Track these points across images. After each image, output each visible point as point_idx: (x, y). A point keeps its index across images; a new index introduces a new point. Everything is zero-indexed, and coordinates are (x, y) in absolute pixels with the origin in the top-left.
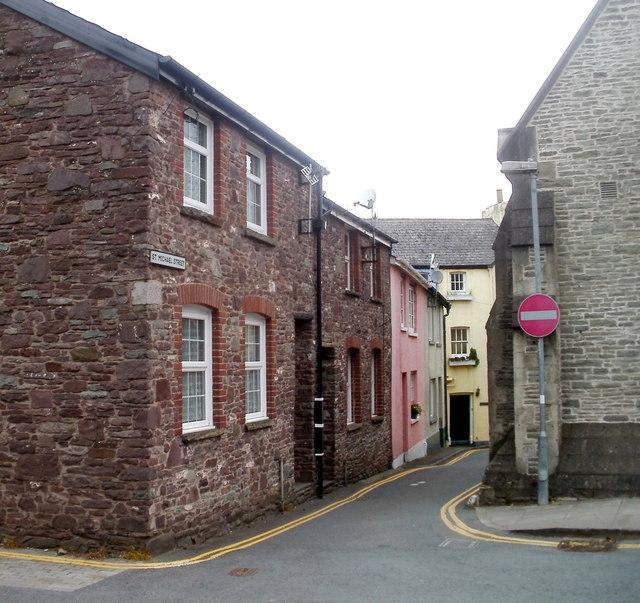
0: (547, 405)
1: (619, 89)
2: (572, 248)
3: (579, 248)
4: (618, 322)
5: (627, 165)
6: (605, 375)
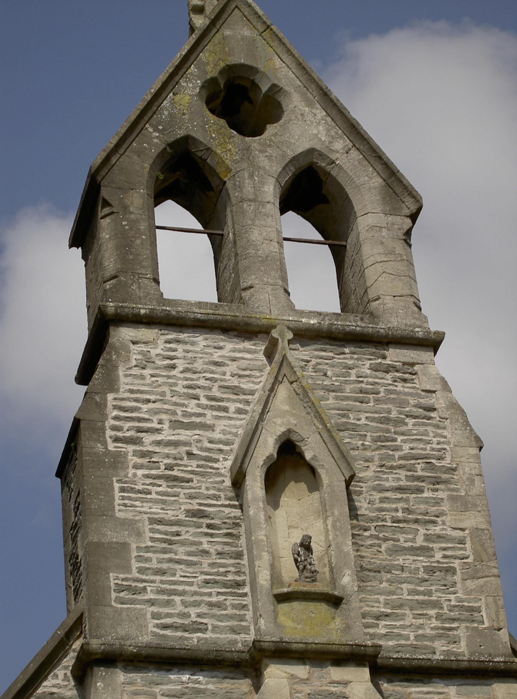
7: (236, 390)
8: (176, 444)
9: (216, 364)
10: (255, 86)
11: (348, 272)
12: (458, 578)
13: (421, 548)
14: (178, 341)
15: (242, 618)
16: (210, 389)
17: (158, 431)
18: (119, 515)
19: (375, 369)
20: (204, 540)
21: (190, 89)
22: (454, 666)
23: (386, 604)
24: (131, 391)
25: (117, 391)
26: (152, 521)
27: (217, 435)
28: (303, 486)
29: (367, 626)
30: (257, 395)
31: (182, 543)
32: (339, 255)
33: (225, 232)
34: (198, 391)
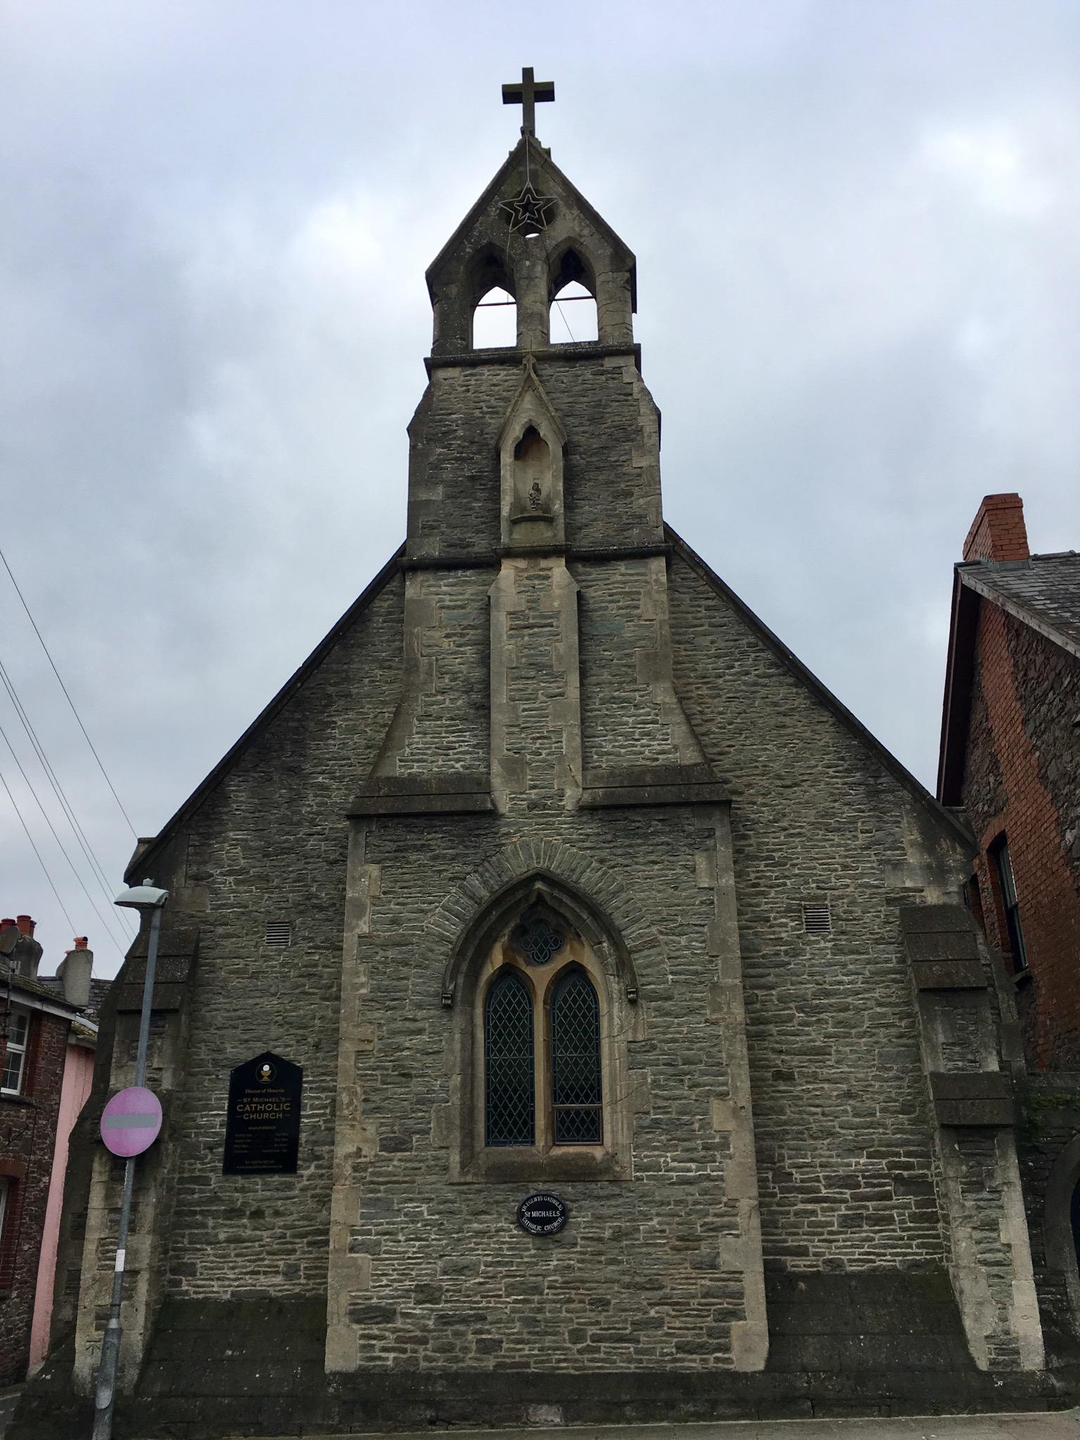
0: (131, 1273)
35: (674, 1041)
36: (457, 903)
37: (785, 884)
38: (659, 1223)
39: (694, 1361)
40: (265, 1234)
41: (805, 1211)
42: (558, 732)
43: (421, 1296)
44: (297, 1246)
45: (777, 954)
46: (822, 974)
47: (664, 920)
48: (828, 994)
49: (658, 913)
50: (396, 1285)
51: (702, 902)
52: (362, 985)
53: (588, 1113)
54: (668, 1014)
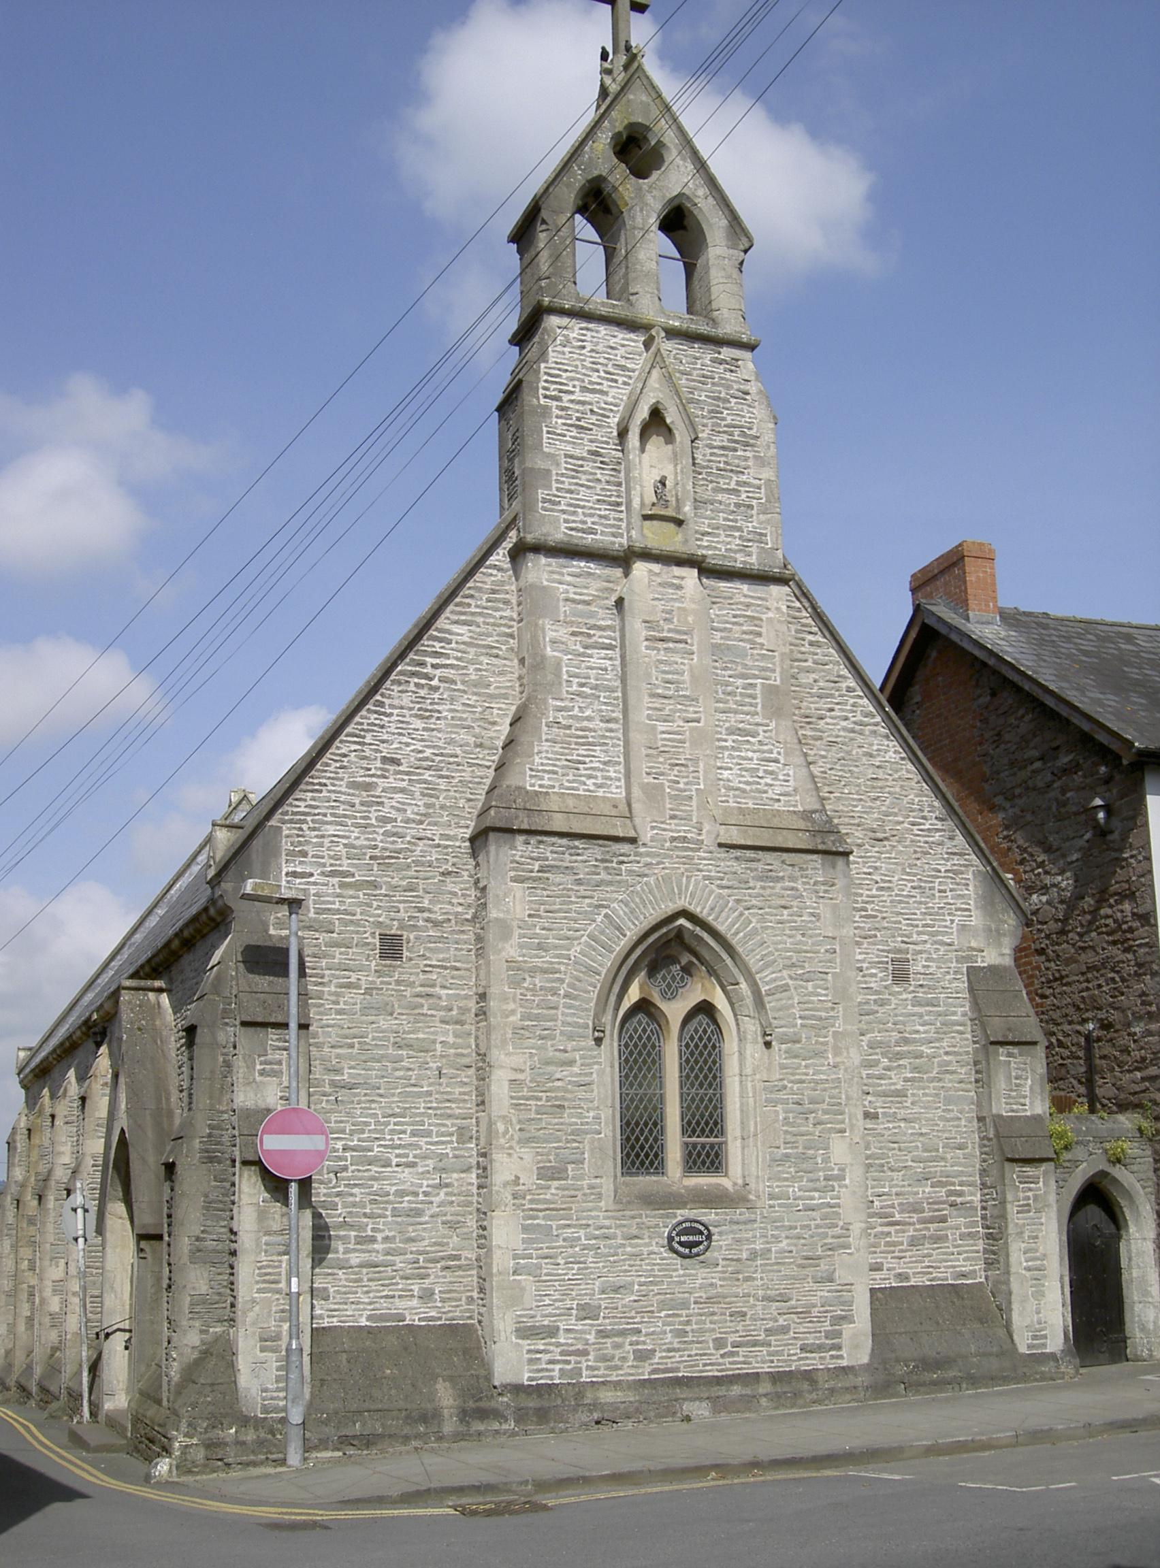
1: (417, 788)
2: (329, 1035)
3: (338, 1036)
4: (395, 1161)
5: (422, 910)
6: (370, 1247)
7: (623, 368)
8: (583, 403)
9: (612, 348)
10: (646, 139)
11: (696, 283)
12: (754, 512)
13: (734, 490)
14: (587, 329)
15: (619, 527)
16: (607, 365)
17: (572, 393)
18: (546, 450)
19: (713, 361)
20: (598, 471)
21: (604, 140)
22: (748, 572)
23: (709, 526)
24: (557, 363)
25: (547, 362)
26: (566, 456)
27: (610, 400)
28: (661, 439)
29: (697, 539)
30: (637, 373)
31: (585, 473)
32: (690, 270)
33: (618, 246)
34: (599, 366)
35: (802, 1082)
36: (602, 932)
37: (876, 936)
38: (788, 1245)
39: (814, 1359)
40: (398, 1259)
41: (882, 1233)
42: (696, 761)
43: (583, 1314)
44: (430, 1271)
45: (867, 1003)
46: (904, 1024)
47: (793, 965)
48: (906, 1041)
49: (790, 958)
50: (557, 1304)
51: (827, 951)
52: (513, 1012)
53: (712, 1146)
54: (796, 1057)
